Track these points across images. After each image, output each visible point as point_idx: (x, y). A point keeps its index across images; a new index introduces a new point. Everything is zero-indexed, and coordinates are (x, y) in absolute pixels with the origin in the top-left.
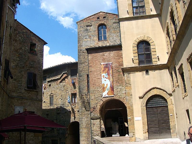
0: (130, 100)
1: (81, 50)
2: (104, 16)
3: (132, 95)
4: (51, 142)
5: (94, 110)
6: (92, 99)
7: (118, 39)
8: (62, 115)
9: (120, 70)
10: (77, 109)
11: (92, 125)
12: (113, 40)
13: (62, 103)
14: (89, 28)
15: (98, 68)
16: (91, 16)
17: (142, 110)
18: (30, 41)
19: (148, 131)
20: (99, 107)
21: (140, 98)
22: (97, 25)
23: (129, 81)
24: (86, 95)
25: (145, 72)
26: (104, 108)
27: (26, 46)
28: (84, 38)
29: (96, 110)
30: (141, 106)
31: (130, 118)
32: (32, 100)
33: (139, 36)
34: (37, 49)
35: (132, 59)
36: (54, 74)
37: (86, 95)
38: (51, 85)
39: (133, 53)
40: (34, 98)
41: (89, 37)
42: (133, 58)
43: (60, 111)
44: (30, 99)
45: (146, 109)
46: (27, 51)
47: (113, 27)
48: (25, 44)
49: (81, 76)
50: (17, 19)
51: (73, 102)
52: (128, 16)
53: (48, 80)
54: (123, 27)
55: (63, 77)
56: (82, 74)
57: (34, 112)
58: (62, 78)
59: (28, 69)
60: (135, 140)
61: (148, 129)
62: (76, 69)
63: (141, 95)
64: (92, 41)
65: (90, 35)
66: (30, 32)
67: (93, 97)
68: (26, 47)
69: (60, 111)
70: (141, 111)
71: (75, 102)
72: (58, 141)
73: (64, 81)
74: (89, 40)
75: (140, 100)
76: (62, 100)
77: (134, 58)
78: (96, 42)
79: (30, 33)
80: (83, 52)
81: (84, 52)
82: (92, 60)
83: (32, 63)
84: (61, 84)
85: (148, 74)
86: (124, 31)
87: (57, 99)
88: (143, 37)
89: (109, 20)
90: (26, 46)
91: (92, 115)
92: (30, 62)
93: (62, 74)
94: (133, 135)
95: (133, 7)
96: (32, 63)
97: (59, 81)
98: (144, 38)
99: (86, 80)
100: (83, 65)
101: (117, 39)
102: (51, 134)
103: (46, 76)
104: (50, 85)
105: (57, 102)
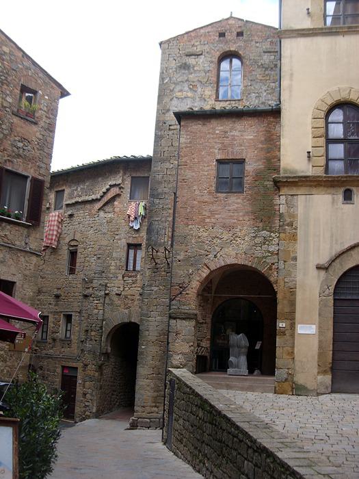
0: (289, 274)
1: (165, 123)
2: (239, 30)
3: (295, 259)
4: (59, 370)
5: (181, 293)
6: (179, 261)
7: (274, 98)
8: (97, 302)
9: (270, 184)
10: (139, 289)
11: (172, 336)
12: (257, 101)
13: (99, 269)
14: (191, 61)
15: (206, 173)
16: (202, 28)
17: (323, 304)
18: (20, 80)
19: (332, 369)
20: (195, 284)
21: (319, 268)
22: (218, 54)
23: (294, 216)
24: (166, 249)
25: (340, 197)
26: (214, 288)
27: (8, 92)
28: (176, 90)
29: (187, 292)
30: (320, 294)
31: (284, 326)
32: (10, 247)
33: (336, 88)
34: (40, 106)
35: (309, 153)
36: (85, 187)
37: (166, 249)
38: (75, 216)
39: (311, 136)
40: (17, 243)
41: (191, 87)
42: (310, 149)
43: (91, 289)
44: (6, 246)
45: (334, 303)
46: (7, 109)
47: (262, 64)
48: (5, 87)
49: (158, 194)
50: (64, 93)
51: (131, 268)
52: (307, 24)
53: (68, 202)
54: (291, 57)
55: (109, 196)
56: (160, 190)
57: (15, 282)
58: (105, 199)
59: (6, 161)
60: (221, 428)
61: (333, 363)
62: (146, 175)
63: (324, 260)
64: (198, 99)
65: (193, 82)
66: (20, 54)
67: (182, 253)
68: (8, 97)
69: (91, 289)
70: (318, 307)
71: (134, 270)
72: (80, 370)
73: (107, 208)
74: (190, 94)
75: (319, 276)
76: (99, 261)
77: (314, 152)
78: (210, 103)
79: (23, 57)
80: (169, 129)
81: (171, 127)
82: (191, 147)
83: (20, 145)
84: (102, 214)
85: (349, 202)
86: (291, 70)
87: (86, 255)
88: (344, 90)
89: (253, 43)
90: (8, 92)
91: (174, 307)
92: (15, 140)
93: (108, 187)
94: (285, 376)
95: (330, 141)
96: (20, 145)
97: (98, 205)
98: (349, 93)
99: (170, 209)
100: (167, 165)
101: (268, 100)
102: (63, 350)
103: (64, 190)
104: (71, 216)
105: (87, 264)
